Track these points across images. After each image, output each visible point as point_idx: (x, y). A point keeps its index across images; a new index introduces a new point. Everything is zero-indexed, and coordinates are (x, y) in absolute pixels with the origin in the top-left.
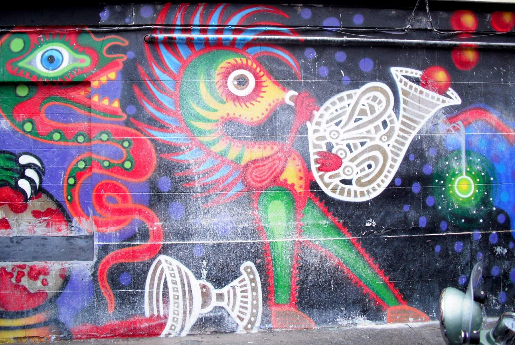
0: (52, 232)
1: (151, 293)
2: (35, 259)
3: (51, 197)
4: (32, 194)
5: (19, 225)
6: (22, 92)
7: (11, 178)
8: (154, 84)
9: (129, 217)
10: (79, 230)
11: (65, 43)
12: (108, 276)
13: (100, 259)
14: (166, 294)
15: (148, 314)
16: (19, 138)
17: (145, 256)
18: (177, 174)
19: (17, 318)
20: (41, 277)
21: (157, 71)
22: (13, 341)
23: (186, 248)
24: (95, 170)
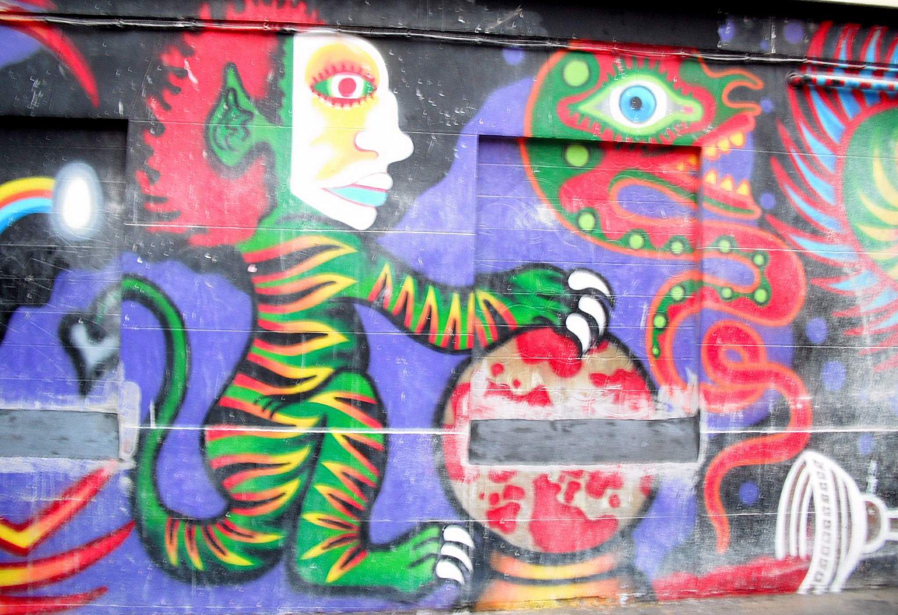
0: (623, 412)
1: (788, 517)
2: (598, 459)
3: (625, 349)
4: (591, 343)
5: (567, 398)
6: (577, 158)
7: (555, 313)
8: (804, 158)
9: (759, 386)
10: (670, 408)
11: (659, 75)
12: (721, 488)
13: (709, 459)
14: (811, 519)
15: (780, 554)
16: (570, 242)
17: (781, 454)
18: (837, 314)
19: (564, 563)
20: (609, 492)
21: (809, 137)
22: (556, 605)
23: (847, 439)
24: (709, 304)
